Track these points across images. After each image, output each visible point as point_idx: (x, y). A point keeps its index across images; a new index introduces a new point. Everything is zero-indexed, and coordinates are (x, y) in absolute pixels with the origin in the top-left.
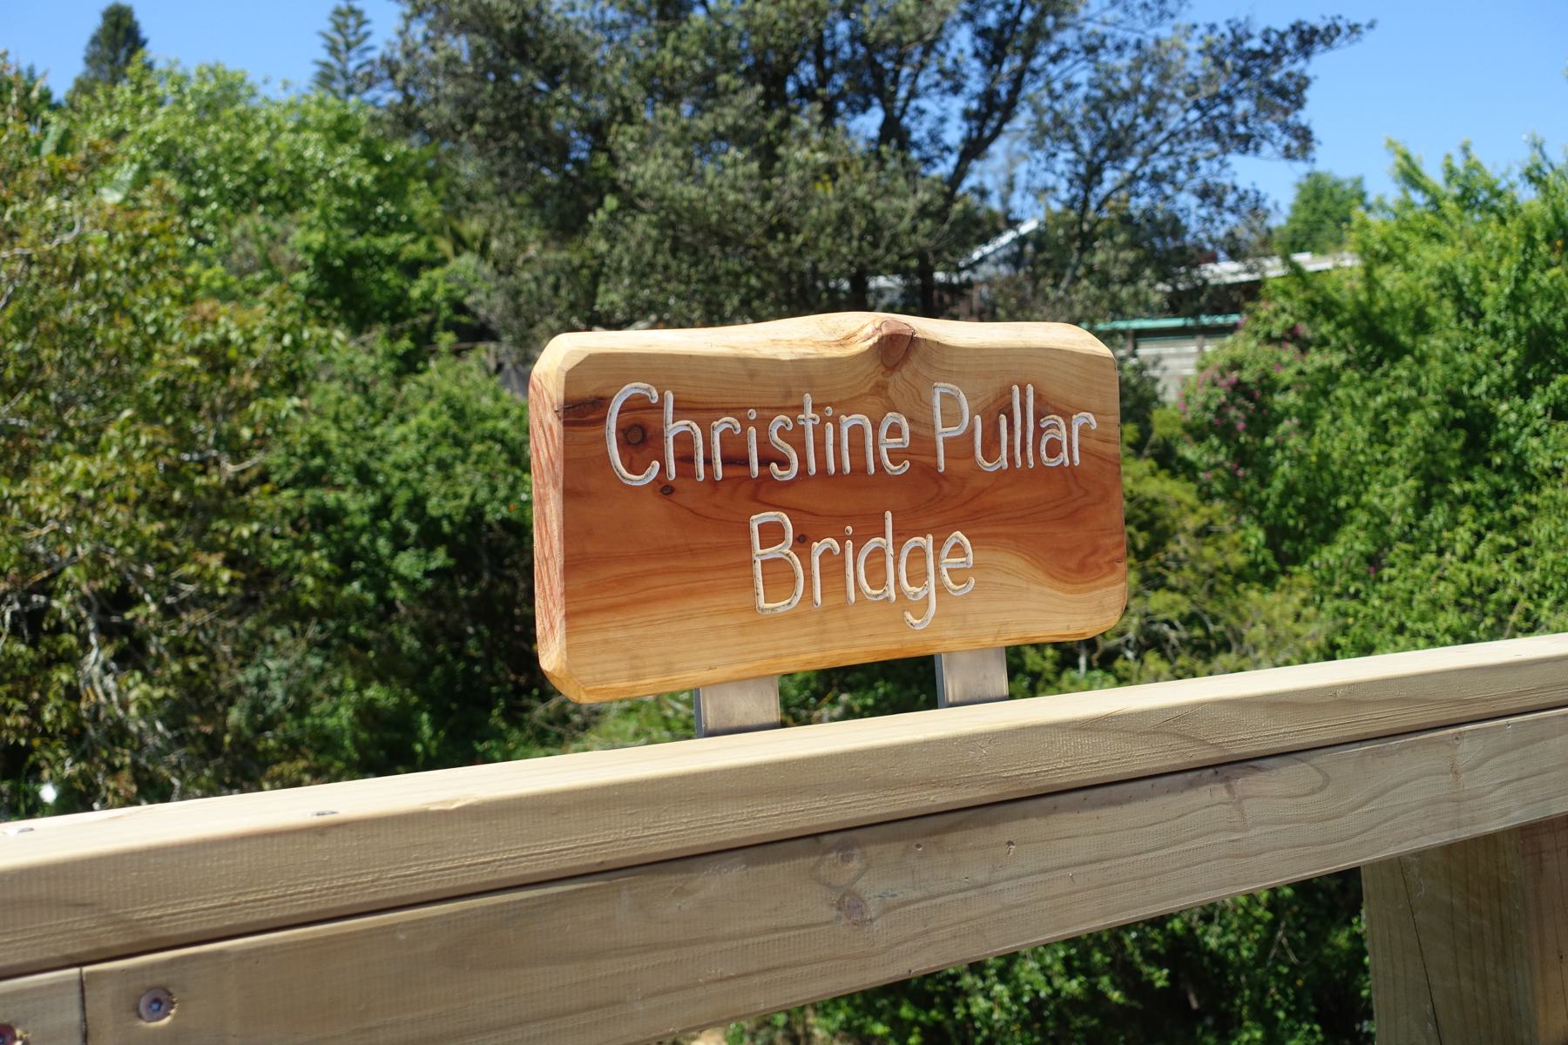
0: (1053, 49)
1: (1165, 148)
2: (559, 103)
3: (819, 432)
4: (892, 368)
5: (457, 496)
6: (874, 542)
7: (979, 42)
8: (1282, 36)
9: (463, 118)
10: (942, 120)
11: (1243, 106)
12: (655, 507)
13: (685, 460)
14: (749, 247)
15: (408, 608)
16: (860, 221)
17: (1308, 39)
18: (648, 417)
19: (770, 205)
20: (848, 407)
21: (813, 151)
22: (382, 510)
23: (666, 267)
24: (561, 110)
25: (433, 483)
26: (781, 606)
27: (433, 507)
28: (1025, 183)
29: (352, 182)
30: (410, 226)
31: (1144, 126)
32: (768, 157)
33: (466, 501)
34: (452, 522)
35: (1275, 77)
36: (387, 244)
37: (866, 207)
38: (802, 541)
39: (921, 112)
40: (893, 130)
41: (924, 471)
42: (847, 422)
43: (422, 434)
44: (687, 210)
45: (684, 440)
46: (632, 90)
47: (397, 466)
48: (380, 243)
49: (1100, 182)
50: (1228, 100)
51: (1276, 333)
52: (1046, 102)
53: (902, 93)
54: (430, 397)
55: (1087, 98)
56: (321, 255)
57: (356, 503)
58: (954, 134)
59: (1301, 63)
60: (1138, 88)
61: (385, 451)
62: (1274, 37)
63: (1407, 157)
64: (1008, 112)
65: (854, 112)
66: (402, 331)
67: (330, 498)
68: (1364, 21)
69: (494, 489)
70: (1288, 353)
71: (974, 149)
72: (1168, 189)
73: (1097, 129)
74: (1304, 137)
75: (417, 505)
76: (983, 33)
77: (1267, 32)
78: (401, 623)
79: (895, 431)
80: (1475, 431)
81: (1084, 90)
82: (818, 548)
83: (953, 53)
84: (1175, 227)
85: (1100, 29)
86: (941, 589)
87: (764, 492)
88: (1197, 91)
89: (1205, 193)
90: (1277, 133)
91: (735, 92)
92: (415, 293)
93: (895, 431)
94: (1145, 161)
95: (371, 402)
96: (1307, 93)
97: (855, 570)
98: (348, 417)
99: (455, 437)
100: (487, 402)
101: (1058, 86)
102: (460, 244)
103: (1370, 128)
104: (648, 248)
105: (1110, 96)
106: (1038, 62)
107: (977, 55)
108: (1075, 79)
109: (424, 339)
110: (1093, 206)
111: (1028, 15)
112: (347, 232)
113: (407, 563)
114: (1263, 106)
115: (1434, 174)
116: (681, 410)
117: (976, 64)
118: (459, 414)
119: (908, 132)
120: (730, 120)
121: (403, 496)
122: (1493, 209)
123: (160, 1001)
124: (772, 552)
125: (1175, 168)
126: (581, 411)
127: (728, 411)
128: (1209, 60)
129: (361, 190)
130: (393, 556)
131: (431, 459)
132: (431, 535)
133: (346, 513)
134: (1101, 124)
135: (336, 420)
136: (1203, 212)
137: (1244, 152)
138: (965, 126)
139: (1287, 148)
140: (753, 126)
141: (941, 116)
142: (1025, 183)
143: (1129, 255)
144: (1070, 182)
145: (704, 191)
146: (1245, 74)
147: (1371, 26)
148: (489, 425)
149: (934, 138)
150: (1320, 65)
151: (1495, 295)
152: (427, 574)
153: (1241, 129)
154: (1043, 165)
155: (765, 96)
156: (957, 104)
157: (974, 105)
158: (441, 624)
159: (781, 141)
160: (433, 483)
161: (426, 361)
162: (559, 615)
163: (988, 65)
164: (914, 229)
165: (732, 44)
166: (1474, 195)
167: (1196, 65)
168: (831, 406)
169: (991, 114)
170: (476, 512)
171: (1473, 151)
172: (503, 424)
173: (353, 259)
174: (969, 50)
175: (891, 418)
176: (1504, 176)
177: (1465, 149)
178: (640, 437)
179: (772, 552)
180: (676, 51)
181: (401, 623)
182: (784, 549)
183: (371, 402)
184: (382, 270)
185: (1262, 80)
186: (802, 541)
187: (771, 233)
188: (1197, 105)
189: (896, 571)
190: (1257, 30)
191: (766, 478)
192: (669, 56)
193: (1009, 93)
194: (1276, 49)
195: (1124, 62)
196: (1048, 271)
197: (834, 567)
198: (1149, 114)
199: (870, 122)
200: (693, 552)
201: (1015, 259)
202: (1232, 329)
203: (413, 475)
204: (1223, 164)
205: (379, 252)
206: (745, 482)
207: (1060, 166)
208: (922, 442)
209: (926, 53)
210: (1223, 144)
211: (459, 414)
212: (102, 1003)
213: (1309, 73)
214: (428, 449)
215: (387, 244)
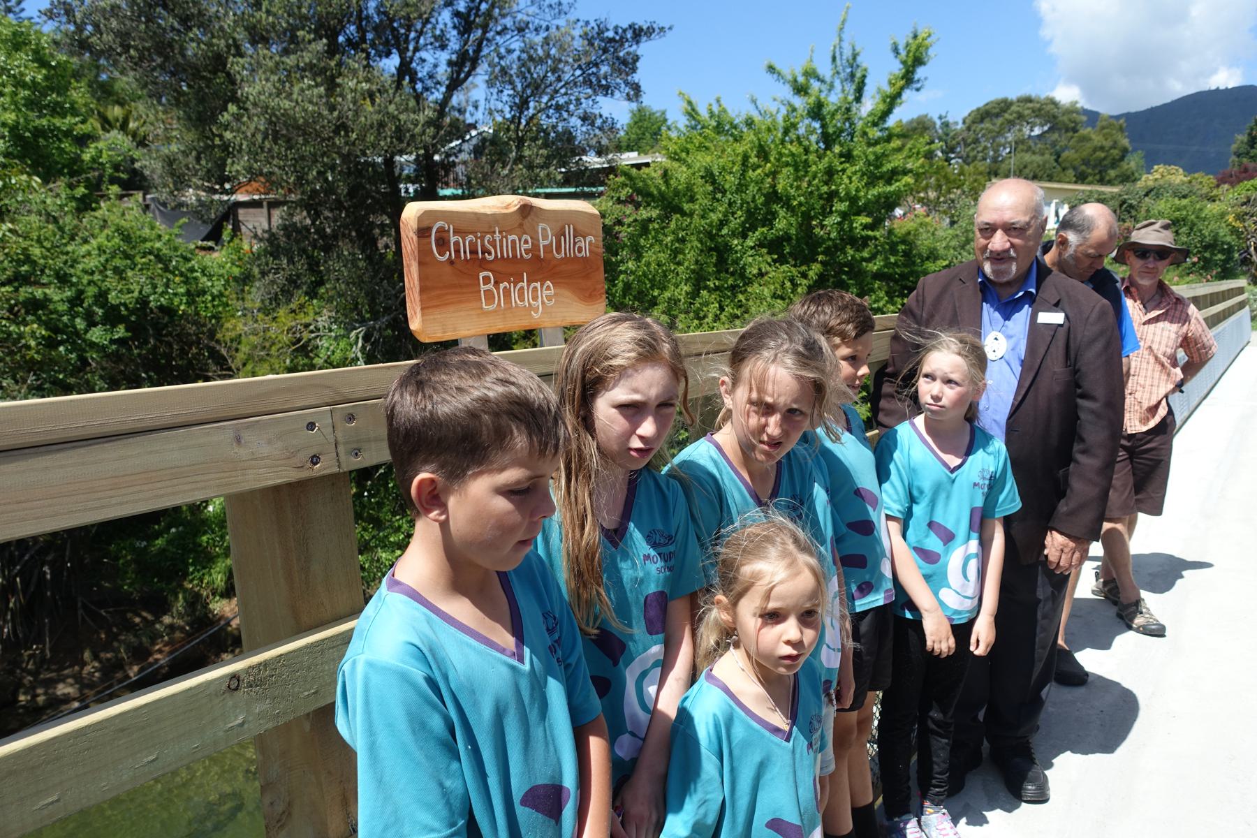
0: (499, 28)
1: (563, 91)
2: (192, 40)
3: (501, 241)
4: (524, 217)
5: (130, 291)
6: (520, 284)
7: (455, 20)
8: (624, 31)
9: (121, 45)
10: (436, 66)
11: (604, 69)
12: (448, 269)
13: (457, 251)
14: (323, 140)
15: (97, 363)
16: (390, 128)
17: (638, 33)
18: (444, 234)
19: (336, 114)
20: (510, 232)
21: (358, 82)
22: (76, 300)
23: (270, 150)
24: (194, 45)
25: (112, 282)
26: (490, 308)
27: (113, 298)
28: (484, 106)
29: (28, 79)
30: (74, 111)
31: (551, 77)
32: (332, 85)
33: (136, 294)
34: (127, 308)
35: (621, 54)
36: (63, 123)
37: (395, 118)
38: (497, 283)
39: (424, 61)
40: (405, 69)
41: (536, 258)
42: (510, 238)
43: (101, 250)
44: (283, 115)
45: (457, 243)
46: (241, 35)
47: (85, 271)
48: (57, 122)
49: (528, 108)
50: (596, 65)
51: (623, 198)
52: (496, 60)
53: (411, 47)
54: (103, 228)
55: (519, 58)
56: (14, 129)
57: (58, 296)
58: (443, 72)
59: (634, 47)
60: (548, 55)
61: (75, 261)
62: (620, 31)
63: (690, 103)
64: (475, 63)
65: (380, 57)
66: (79, 182)
67: (39, 293)
68: (667, 26)
69: (155, 287)
70: (629, 209)
71: (455, 84)
72: (565, 115)
73: (526, 78)
74: (637, 88)
75: (102, 297)
76: (457, 14)
77: (616, 27)
78: (93, 373)
79: (526, 242)
80: (720, 253)
81: (517, 53)
82: (502, 286)
83: (441, 26)
84: (568, 136)
85: (529, 19)
86: (543, 303)
87: (484, 264)
88: (580, 60)
89: (584, 118)
90: (623, 86)
91: (310, 42)
92: (86, 157)
93: (526, 242)
94: (552, 98)
95: (61, 229)
96: (638, 64)
97: (515, 296)
98: (46, 239)
99: (124, 252)
100: (146, 232)
101: (502, 50)
102: (107, 124)
103: (672, 84)
104: (259, 137)
105: (531, 58)
106: (490, 35)
107: (455, 27)
108: (512, 47)
109: (95, 188)
110: (523, 122)
111: (484, 6)
112: (32, 115)
113: (97, 334)
114: (616, 71)
115: (704, 113)
116: (455, 232)
117: (455, 32)
118: (127, 238)
119: (416, 73)
120: (307, 60)
121: (91, 291)
122: (732, 135)
123: (351, 418)
124: (487, 287)
125: (568, 103)
126: (423, 232)
127: (471, 233)
128: (586, 42)
129: (34, 85)
130: (86, 331)
131: (108, 267)
132: (113, 316)
133: (50, 301)
134: (528, 75)
135: (39, 241)
136: (584, 129)
137: (606, 95)
138: (449, 70)
139: (628, 94)
140: (323, 64)
141: (435, 62)
142: (484, 106)
143: (544, 152)
144: (511, 107)
145: (293, 104)
146: (605, 51)
147: (670, 28)
148: (148, 245)
149: (431, 76)
150: (644, 49)
151: (730, 181)
152: (112, 341)
153: (604, 82)
154: (495, 96)
155: (329, 45)
156: (444, 56)
157: (454, 57)
158: (122, 372)
159: (340, 74)
160: (112, 282)
161: (97, 203)
162: (418, 310)
163: (461, 34)
164: (424, 133)
165: (304, 11)
166: (722, 126)
167: (579, 44)
168: (505, 232)
169: (463, 65)
170: (143, 301)
171: (722, 102)
172: (158, 245)
173: (39, 132)
174: (450, 25)
175: (525, 237)
176: (738, 116)
177: (718, 101)
178: (442, 243)
179: (487, 287)
180: (268, 12)
181: (93, 373)
182: (491, 286)
183: (61, 229)
184: (60, 140)
185: (614, 54)
186: (497, 283)
187: (336, 132)
188: (580, 67)
189: (528, 295)
190: (611, 27)
191: (484, 258)
192: (264, 16)
193: (474, 51)
194: (622, 38)
195: (538, 39)
196: (498, 160)
197: (507, 293)
198: (554, 71)
199: (391, 63)
200: (461, 286)
201: (478, 151)
202: (601, 194)
203: (97, 277)
204: (595, 102)
205: (59, 129)
206: (478, 261)
207: (505, 98)
208: (535, 246)
209: (424, 25)
210: (595, 91)
211: (127, 238)
212: (337, 416)
213: (639, 53)
214: (107, 260)
215: (63, 123)
